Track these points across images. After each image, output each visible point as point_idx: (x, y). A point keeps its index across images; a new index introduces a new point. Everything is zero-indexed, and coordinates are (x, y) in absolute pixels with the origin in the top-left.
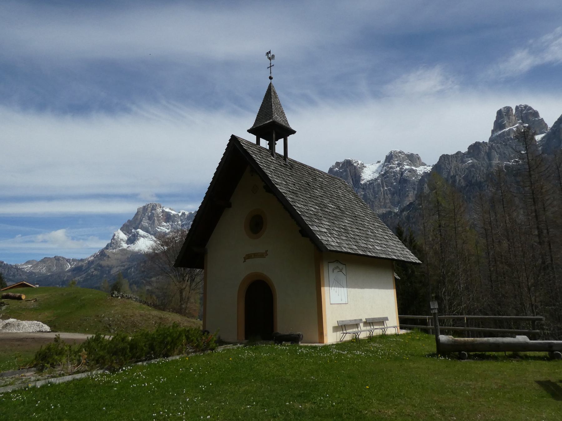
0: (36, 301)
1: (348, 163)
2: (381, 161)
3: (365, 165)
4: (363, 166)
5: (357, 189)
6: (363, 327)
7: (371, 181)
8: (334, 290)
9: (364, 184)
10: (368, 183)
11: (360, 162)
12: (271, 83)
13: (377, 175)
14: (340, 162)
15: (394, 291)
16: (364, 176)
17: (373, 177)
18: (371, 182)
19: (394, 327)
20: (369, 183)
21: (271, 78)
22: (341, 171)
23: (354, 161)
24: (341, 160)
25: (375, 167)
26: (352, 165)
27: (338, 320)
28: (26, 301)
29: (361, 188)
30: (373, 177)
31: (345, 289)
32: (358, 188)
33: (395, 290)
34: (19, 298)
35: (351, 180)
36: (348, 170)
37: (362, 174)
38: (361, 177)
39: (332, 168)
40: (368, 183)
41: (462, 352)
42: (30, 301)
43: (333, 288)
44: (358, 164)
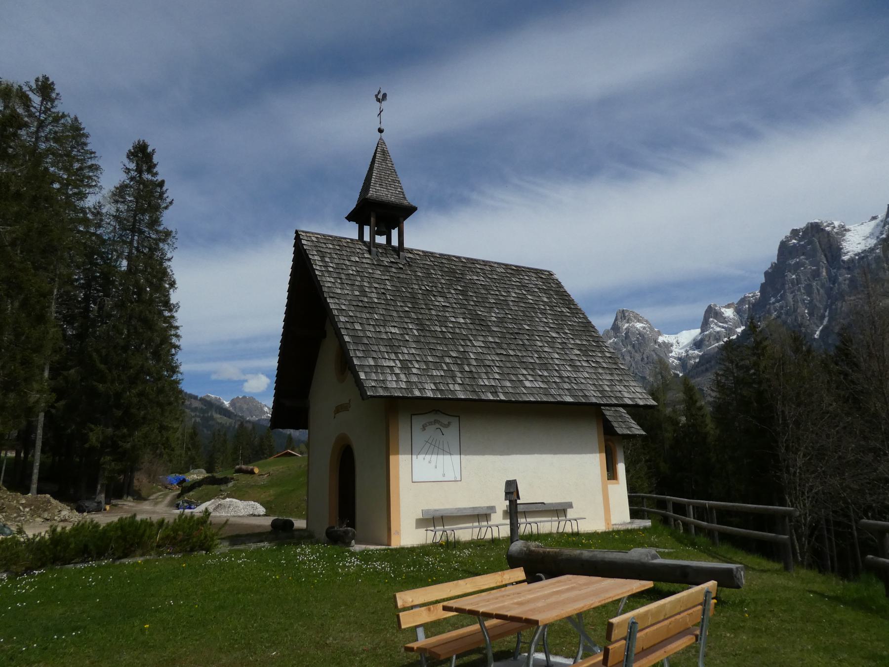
0: (269, 475)
1: (815, 229)
2: (879, 216)
3: (847, 227)
4: (843, 230)
5: (835, 270)
6: (503, 519)
7: (862, 253)
8: (424, 459)
9: (849, 260)
10: (857, 257)
11: (836, 224)
12: (381, 139)
13: (872, 242)
14: (799, 230)
15: (600, 458)
16: (847, 247)
17: (866, 246)
18: (863, 255)
19: (575, 520)
20: (859, 258)
21: (381, 131)
22: (802, 243)
23: (825, 224)
24: (801, 225)
25: (869, 227)
26: (823, 230)
27: (423, 509)
28: (259, 475)
29: (845, 268)
30: (866, 246)
31: (456, 458)
32: (839, 269)
33: (604, 455)
34: (252, 472)
35: (823, 256)
36: (816, 240)
37: (844, 244)
38: (842, 248)
39: (785, 241)
40: (857, 257)
41: (537, 574)
42: (263, 475)
43: (421, 457)
44: (834, 227)
